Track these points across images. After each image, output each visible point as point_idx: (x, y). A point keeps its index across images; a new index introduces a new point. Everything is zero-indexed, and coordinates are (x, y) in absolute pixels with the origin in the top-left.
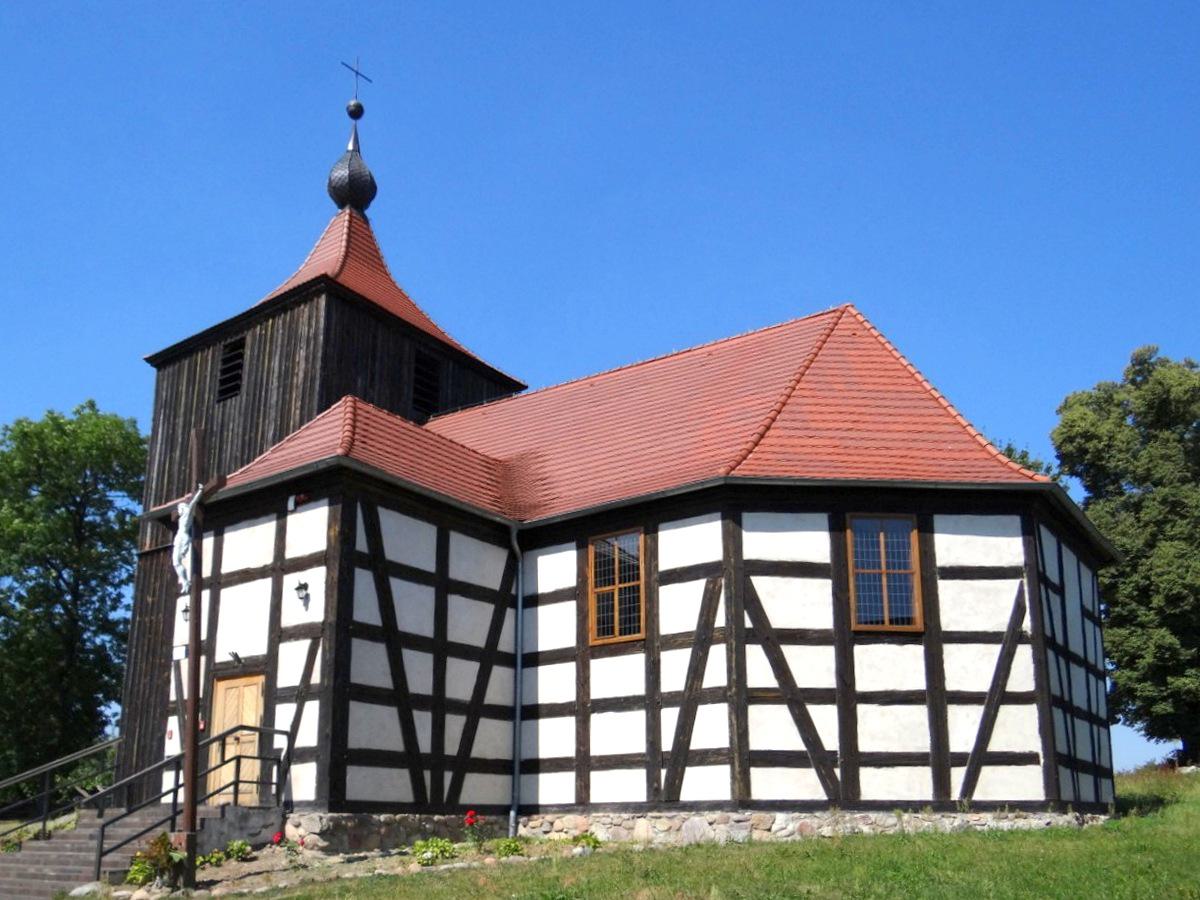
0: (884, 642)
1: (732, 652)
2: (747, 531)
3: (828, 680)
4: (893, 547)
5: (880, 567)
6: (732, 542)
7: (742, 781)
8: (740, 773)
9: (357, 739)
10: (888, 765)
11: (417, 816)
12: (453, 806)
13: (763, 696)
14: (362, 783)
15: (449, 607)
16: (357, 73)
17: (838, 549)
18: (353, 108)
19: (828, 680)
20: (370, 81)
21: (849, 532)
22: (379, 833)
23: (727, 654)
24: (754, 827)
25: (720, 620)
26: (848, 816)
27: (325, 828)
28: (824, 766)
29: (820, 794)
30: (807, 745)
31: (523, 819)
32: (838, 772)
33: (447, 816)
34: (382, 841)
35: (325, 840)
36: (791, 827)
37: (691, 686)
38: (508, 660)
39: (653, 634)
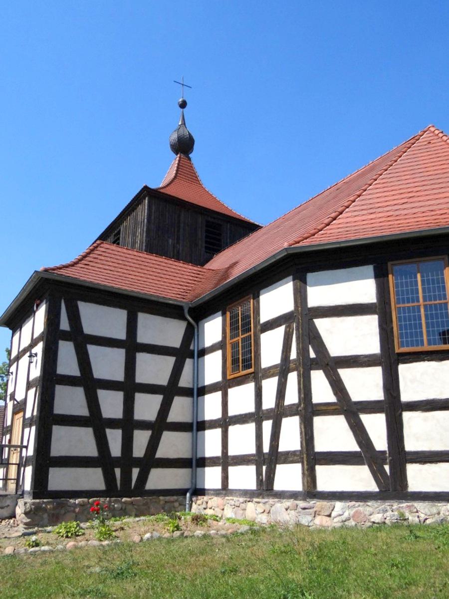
0: (424, 360)
1: (300, 377)
2: (310, 286)
3: (377, 393)
4: (439, 287)
5: (418, 301)
6: (300, 296)
7: (310, 477)
8: (307, 470)
9: (58, 449)
10: (431, 462)
11: (108, 499)
12: (140, 489)
13: (325, 410)
14: (59, 479)
15: (137, 360)
16: (183, 85)
17: (382, 291)
18: (181, 103)
19: (377, 393)
20: (191, 87)
21: (390, 276)
22: (74, 511)
23: (298, 378)
24: (316, 514)
25: (293, 355)
26: (396, 505)
27: (28, 510)
28: (375, 463)
29: (373, 487)
30: (360, 447)
31: (194, 499)
32: (387, 468)
33: (132, 498)
34: (76, 516)
35: (28, 518)
36: (346, 515)
37: (279, 404)
38: (187, 392)
39: (258, 368)
